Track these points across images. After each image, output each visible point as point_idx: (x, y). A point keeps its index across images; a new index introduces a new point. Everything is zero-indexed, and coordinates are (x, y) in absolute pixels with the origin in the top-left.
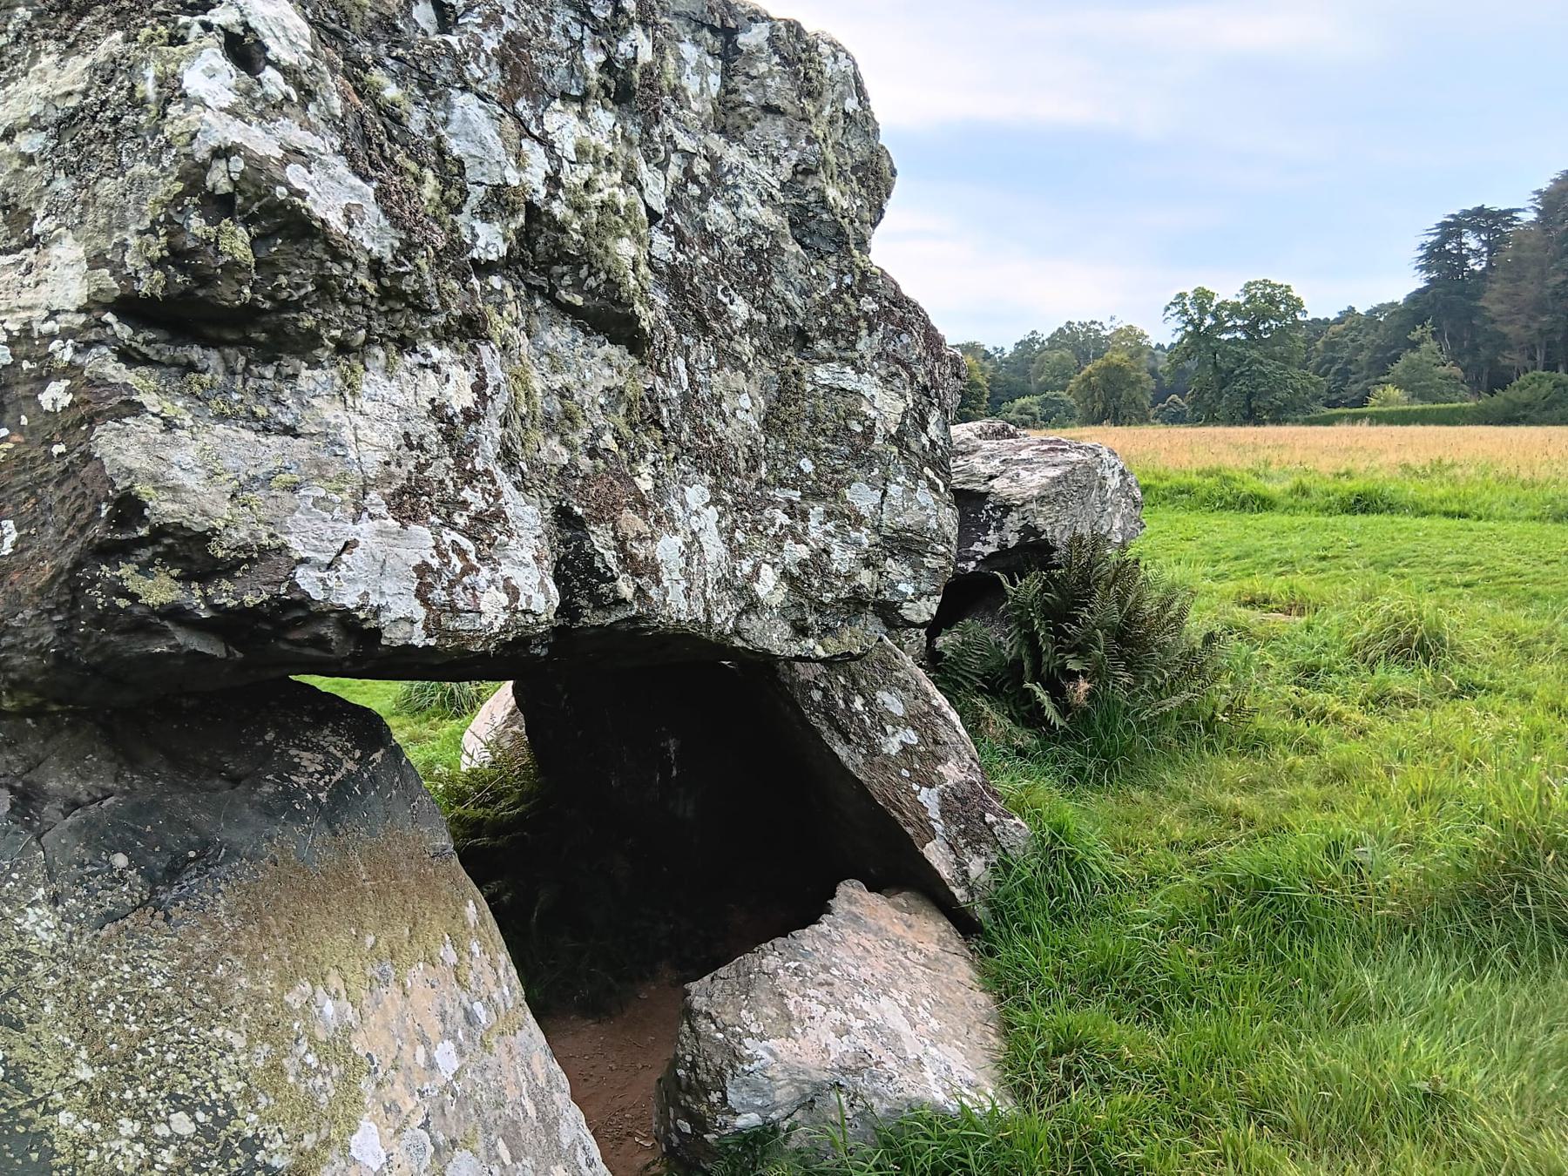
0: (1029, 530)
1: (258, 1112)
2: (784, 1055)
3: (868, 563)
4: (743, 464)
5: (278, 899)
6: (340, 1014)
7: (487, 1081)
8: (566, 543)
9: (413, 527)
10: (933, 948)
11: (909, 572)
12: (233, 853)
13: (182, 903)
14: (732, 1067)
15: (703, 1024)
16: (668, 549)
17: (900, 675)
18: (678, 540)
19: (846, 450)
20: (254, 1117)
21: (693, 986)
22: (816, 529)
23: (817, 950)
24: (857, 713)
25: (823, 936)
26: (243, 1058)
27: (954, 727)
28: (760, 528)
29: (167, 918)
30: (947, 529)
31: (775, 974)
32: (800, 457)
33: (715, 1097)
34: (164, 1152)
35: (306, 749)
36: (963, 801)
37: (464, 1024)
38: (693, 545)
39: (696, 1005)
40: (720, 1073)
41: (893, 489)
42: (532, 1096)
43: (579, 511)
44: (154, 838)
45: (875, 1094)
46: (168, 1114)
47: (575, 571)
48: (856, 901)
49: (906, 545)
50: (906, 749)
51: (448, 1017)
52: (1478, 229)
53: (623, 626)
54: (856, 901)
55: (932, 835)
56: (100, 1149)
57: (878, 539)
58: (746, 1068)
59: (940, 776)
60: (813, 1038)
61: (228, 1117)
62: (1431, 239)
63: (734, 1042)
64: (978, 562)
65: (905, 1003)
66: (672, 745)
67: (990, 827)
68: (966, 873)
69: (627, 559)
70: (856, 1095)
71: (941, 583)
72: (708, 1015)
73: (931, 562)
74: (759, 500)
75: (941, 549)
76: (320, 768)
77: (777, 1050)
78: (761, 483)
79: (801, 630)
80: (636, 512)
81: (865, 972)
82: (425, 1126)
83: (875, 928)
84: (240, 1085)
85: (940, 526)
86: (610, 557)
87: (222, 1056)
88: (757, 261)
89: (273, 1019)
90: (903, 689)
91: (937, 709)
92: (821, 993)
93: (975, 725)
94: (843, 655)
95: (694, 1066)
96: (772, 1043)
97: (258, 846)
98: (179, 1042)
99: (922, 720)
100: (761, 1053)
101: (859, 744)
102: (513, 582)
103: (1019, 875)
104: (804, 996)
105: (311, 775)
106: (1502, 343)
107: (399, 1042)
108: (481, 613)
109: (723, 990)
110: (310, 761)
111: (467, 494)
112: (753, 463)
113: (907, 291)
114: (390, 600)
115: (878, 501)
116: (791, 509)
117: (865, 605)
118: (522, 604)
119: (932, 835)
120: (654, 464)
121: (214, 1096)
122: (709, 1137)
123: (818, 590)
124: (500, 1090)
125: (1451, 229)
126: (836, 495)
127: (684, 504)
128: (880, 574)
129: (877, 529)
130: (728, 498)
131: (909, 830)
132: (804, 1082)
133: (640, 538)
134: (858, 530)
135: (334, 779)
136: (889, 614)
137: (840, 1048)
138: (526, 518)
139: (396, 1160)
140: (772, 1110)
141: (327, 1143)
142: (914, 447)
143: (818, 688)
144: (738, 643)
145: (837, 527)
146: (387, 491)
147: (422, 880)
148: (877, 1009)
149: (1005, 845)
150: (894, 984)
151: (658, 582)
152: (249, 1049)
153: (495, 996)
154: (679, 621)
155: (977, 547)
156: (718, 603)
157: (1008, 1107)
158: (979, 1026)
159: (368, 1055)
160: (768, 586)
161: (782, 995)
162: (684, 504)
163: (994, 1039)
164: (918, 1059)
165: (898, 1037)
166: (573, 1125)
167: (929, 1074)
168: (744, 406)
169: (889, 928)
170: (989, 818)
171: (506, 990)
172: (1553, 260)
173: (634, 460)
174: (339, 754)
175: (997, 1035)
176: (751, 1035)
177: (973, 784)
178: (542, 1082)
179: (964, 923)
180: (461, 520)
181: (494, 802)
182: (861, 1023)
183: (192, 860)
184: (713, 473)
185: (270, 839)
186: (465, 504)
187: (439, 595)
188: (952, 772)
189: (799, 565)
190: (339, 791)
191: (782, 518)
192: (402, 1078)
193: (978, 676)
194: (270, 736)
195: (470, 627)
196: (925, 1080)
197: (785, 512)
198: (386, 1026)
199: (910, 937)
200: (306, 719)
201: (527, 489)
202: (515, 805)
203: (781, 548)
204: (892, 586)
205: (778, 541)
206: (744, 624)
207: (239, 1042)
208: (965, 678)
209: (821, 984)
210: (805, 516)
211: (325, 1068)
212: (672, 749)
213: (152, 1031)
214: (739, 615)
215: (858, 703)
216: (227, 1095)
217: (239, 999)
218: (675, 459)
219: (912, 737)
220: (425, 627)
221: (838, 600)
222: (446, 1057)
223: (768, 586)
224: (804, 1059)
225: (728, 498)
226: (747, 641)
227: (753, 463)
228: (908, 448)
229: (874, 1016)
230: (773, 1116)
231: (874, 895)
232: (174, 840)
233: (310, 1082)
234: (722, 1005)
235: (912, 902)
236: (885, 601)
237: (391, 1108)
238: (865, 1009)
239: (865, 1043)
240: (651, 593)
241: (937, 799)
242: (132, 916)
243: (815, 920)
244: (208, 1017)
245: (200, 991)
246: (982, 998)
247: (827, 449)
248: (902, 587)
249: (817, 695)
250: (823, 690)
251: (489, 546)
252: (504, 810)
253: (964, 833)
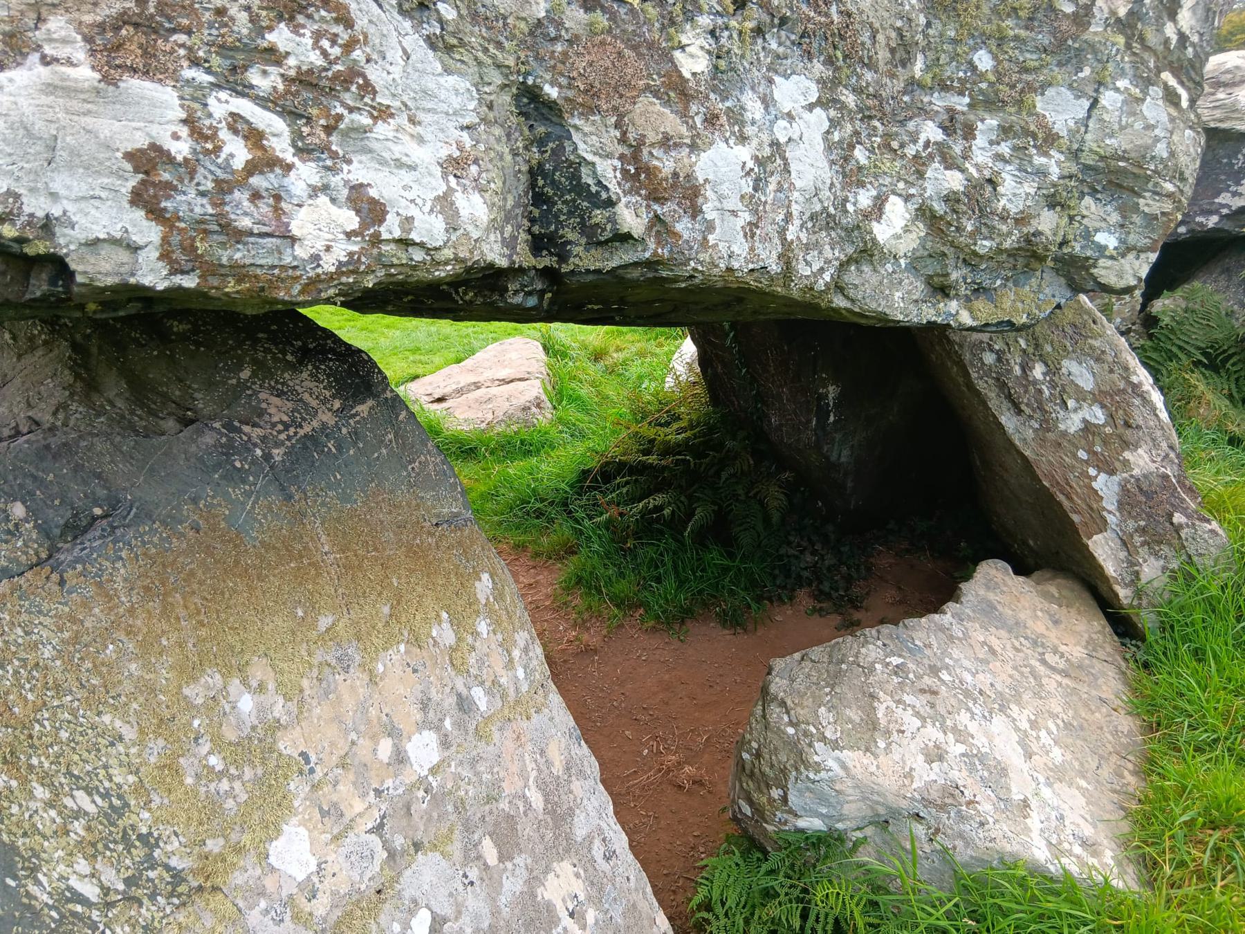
1: (150, 810)
2: (858, 772)
3: (1053, 202)
4: (883, 55)
5: (192, 574)
6: (261, 709)
7: (477, 774)
8: (541, 142)
9: (134, 84)
10: (1077, 652)
11: (1115, 218)
12: (146, 515)
13: (79, 567)
14: (797, 769)
15: (775, 711)
16: (721, 165)
17: (1096, 343)
18: (744, 154)
19: (1044, 39)
20: (146, 815)
21: (779, 664)
22: (982, 153)
23: (930, 646)
24: (1035, 382)
25: (942, 629)
26: (133, 750)
27: (1154, 410)
28: (895, 145)
29: (62, 582)
30: (1183, 160)
31: (872, 670)
32: (975, 49)
33: (776, 793)
34: (76, 823)
35: (280, 395)
36: (1149, 495)
37: (455, 712)
38: (773, 160)
39: (773, 689)
40: (784, 771)
41: (1109, 99)
42: (542, 787)
43: (552, 92)
44: (56, 489)
45: (961, 835)
46: (72, 789)
47: (551, 195)
48: (997, 586)
49: (1116, 179)
50: (1088, 428)
51: (432, 705)
53: (635, 274)
54: (997, 586)
55: (1102, 526)
56: (20, 806)
57: (1074, 169)
58: (812, 776)
59: (1126, 463)
60: (897, 757)
61: (123, 808)
63: (804, 742)
64: (1222, 217)
65: (1025, 725)
66: (832, 391)
67: (1177, 529)
68: (1137, 574)
69: (638, 174)
70: (937, 830)
71: (1160, 236)
72: (783, 704)
73: (1149, 204)
74: (908, 107)
75: (1169, 187)
76: (285, 418)
77: (850, 764)
78: (913, 84)
79: (942, 290)
80: (667, 103)
81: (984, 680)
82: (378, 829)
83: (1011, 622)
84: (132, 779)
85: (1172, 154)
86: (608, 171)
87: (112, 744)
89: (167, 714)
90: (1098, 360)
91: (1136, 387)
92: (919, 702)
93: (1180, 405)
94: (1000, 323)
95: (758, 755)
96: (846, 755)
97: (178, 508)
98: (69, 722)
99: (1116, 397)
100: (831, 763)
101: (1031, 417)
102: (373, 193)
103: (1203, 589)
104: (899, 702)
105: (274, 425)
107: (353, 736)
108: (293, 240)
109: (808, 676)
110: (277, 409)
111: (280, 37)
112: (903, 52)
114: (71, 208)
115: (1082, 114)
116: (951, 123)
117: (1041, 259)
118: (391, 228)
119: (1102, 526)
120: (712, 33)
121: (107, 784)
122: (770, 828)
123: (972, 235)
124: (497, 784)
126: (1020, 103)
127: (767, 101)
128: (1071, 218)
129: (1075, 155)
130: (850, 99)
131: (1076, 518)
132: (878, 803)
133: (667, 143)
134: (1046, 154)
135: (301, 432)
136: (1076, 272)
137: (926, 775)
138: (443, 95)
139: (330, 869)
140: (839, 821)
141: (239, 850)
142: (1152, 39)
143: (992, 351)
144: (840, 302)
145: (1015, 148)
146: (88, 18)
147: (414, 552)
148: (987, 734)
149: (1192, 552)
150: (1018, 698)
151: (695, 212)
152: (141, 743)
153: (503, 680)
154: (730, 270)
155: (1225, 198)
156: (807, 248)
157: (1125, 881)
158: (1114, 758)
159: (303, 755)
160: (895, 226)
161: (873, 697)
162: (767, 101)
163: (1130, 779)
164: (1025, 801)
165: (1004, 772)
166: (594, 811)
167: (1034, 822)
169: (1030, 623)
170: (1178, 518)
171: (521, 673)
173: (673, 22)
174: (314, 403)
175: (1134, 773)
176: (823, 739)
177: (1165, 477)
178: (558, 768)
179: (1123, 626)
180: (264, 80)
181: (667, 424)
182: (961, 748)
183: (99, 517)
184: (830, 61)
185: (195, 500)
186: (273, 56)
187: (190, 203)
188: (1141, 460)
189: (947, 199)
190: (305, 447)
191: (931, 132)
192: (351, 777)
193: (1198, 348)
194: (245, 374)
195: (269, 261)
196: (1027, 830)
197: (941, 126)
198: (338, 719)
199: (1053, 636)
200: (289, 357)
201: (449, 49)
202: (684, 430)
203: (921, 175)
204: (1087, 235)
205: (919, 166)
206: (852, 276)
207: (129, 733)
208: (1180, 348)
209: (923, 691)
210: (969, 133)
211: (233, 771)
212: (831, 396)
213: (45, 704)
214: (843, 266)
215: (1038, 371)
216: (119, 786)
217: (128, 687)
218: (759, 31)
219: (1098, 416)
220: (165, 256)
221: (1000, 251)
222: (423, 750)
223: (895, 226)
224: (880, 780)
225: (850, 99)
226: (853, 301)
227: (903, 52)
228: (1142, 39)
229: (980, 741)
230: (840, 826)
231: (1021, 579)
232: (77, 492)
233: (212, 786)
234: (802, 696)
235: (1065, 592)
236: (1071, 256)
237: (331, 812)
238: (975, 727)
239: (959, 775)
240: (679, 227)
241: (1116, 489)
242: (29, 575)
243: (936, 608)
244: (94, 701)
245: (88, 671)
246: (1126, 723)
247: (1016, 38)
248: (1101, 238)
249: (989, 358)
250: (997, 352)
251: (329, 130)
252: (671, 435)
253: (1142, 531)
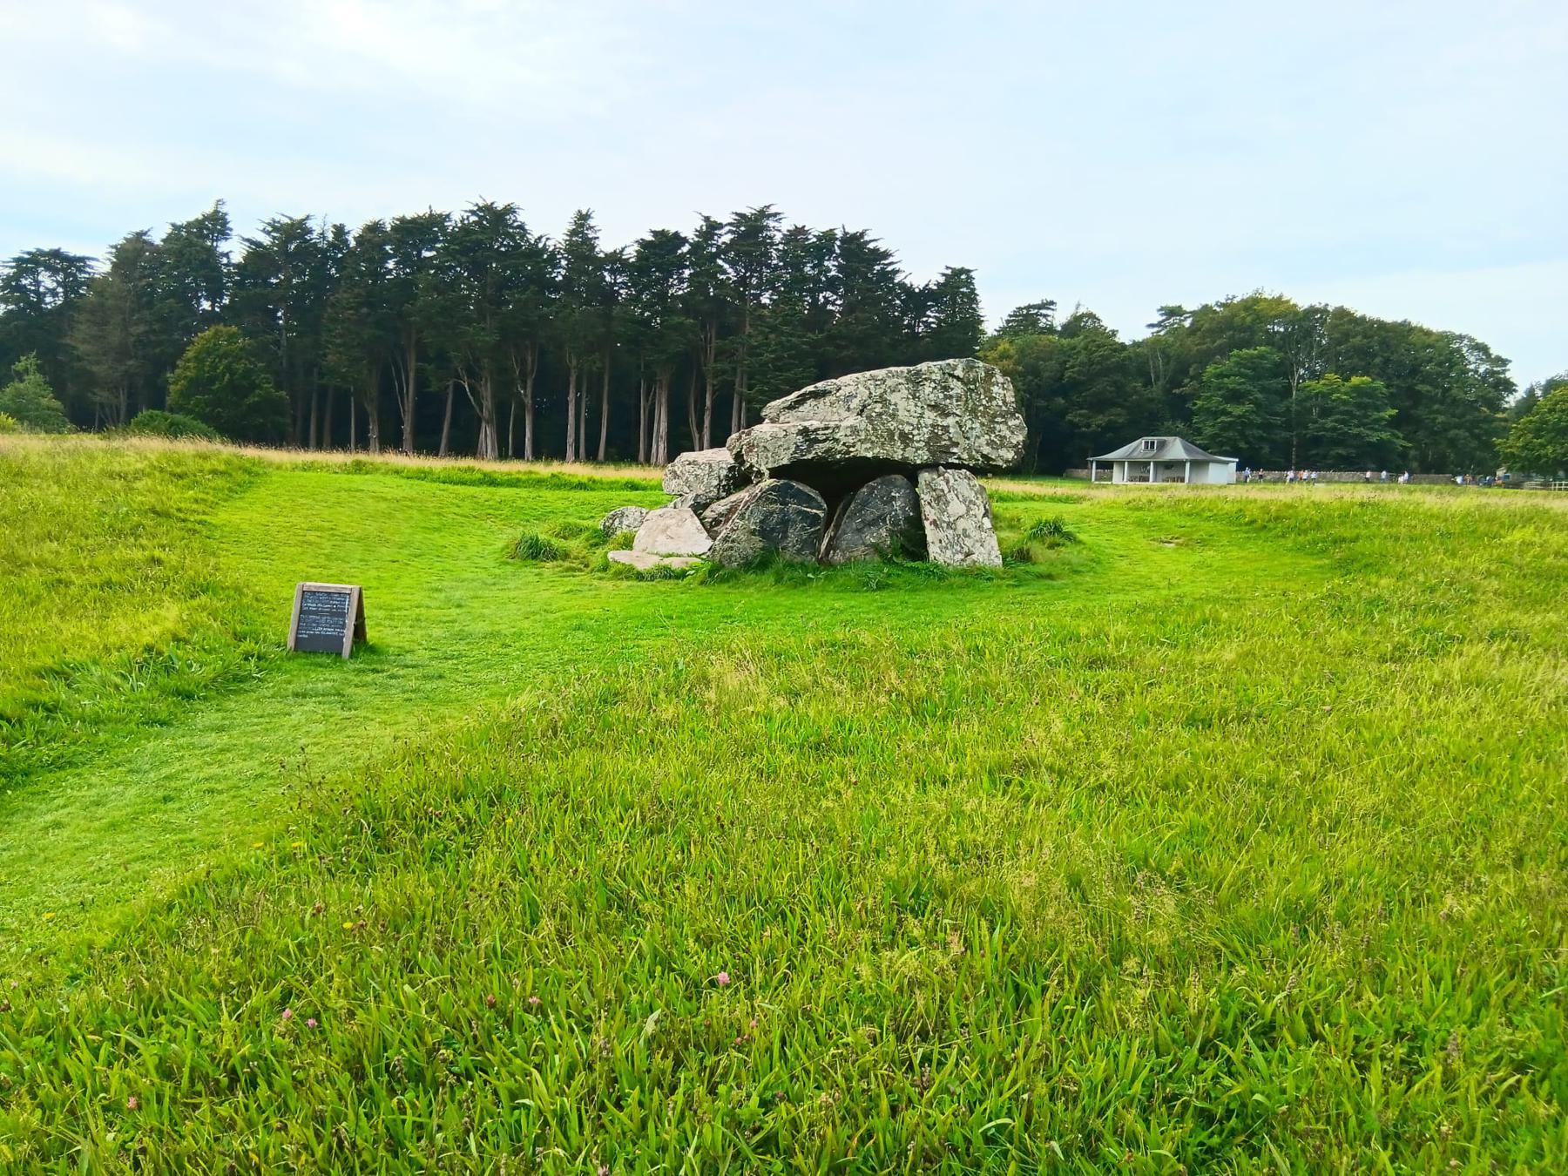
52: (54, 271)
62: (7, 271)
106: (91, 381)
113: (1303, 300)
125: (29, 264)
172: (133, 311)
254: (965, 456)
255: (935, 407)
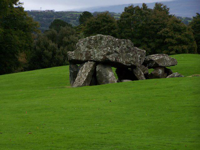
0: (156, 63)
47: (116, 60)
88: (125, 49)
99: (141, 73)
168: (124, 55)
254: (94, 58)
255: (87, 47)
